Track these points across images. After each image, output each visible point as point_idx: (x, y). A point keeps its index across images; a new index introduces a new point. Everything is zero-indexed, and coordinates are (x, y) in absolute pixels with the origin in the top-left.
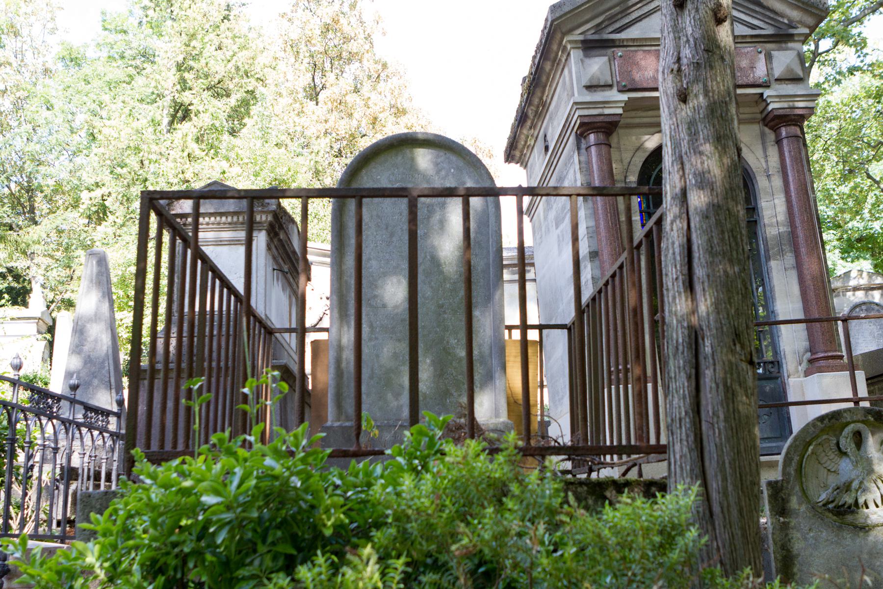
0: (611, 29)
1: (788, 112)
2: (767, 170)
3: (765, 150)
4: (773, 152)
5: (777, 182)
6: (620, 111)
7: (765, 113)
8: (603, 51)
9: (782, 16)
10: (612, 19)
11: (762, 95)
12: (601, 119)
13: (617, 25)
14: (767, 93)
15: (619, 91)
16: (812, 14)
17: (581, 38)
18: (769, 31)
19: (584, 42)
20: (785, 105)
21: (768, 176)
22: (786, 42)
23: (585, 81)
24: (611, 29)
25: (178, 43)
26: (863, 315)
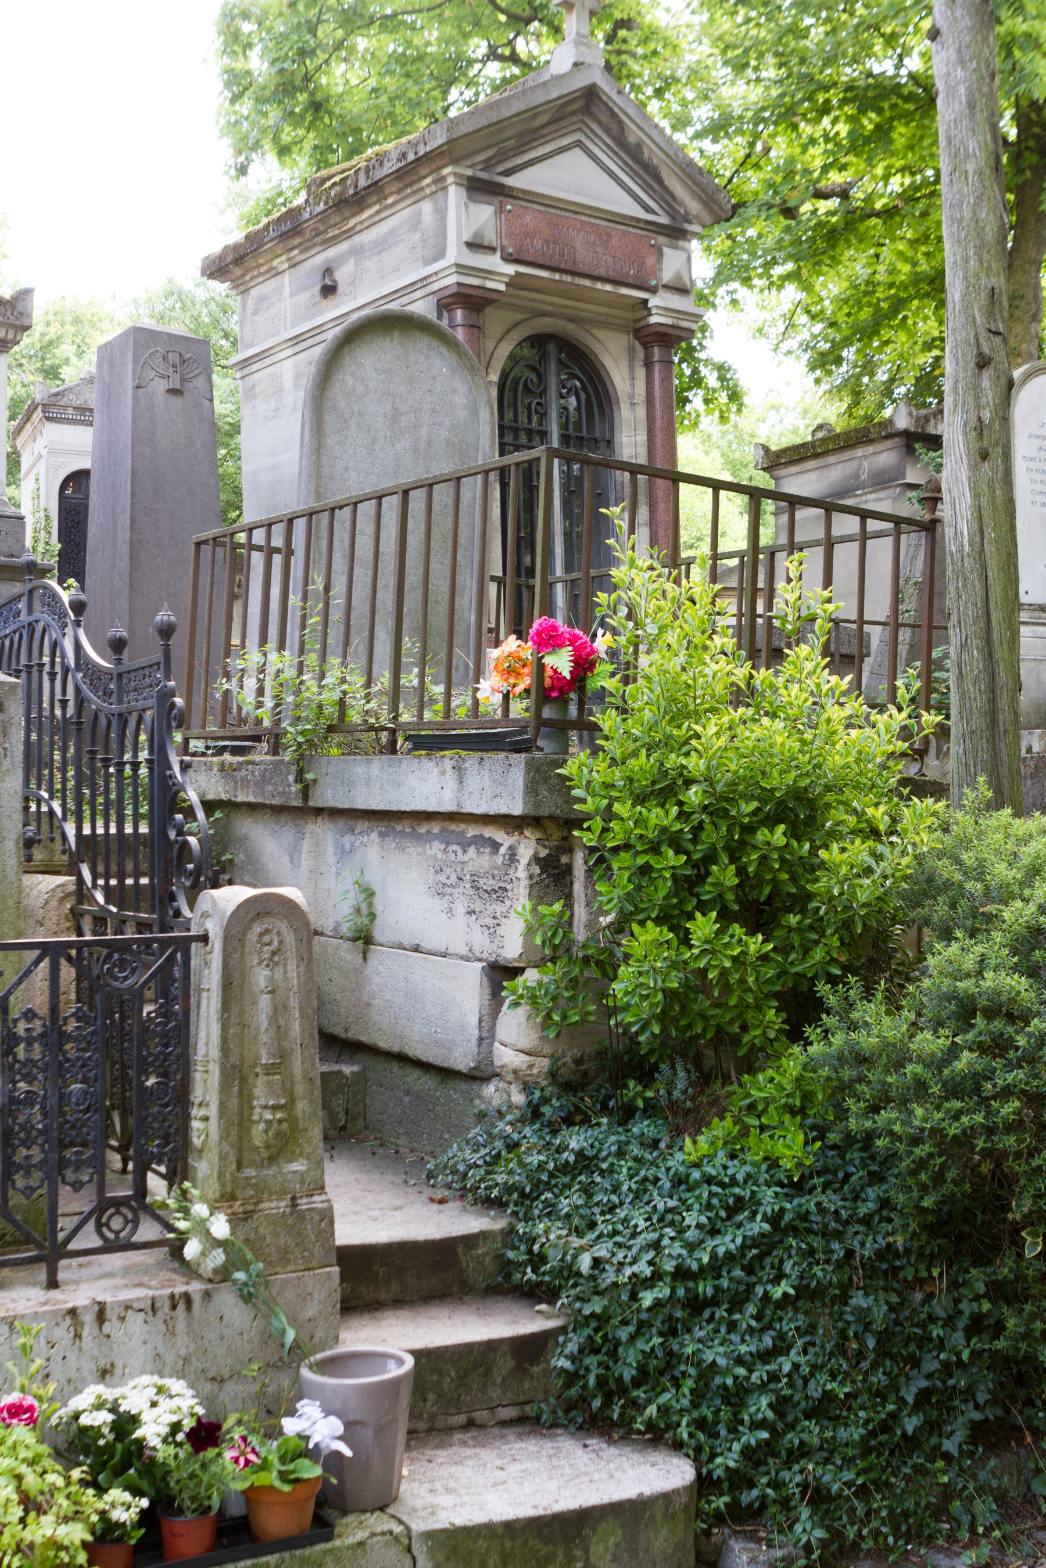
0: (500, 168)
1: (670, 331)
2: (631, 396)
3: (632, 369)
4: (641, 373)
5: (641, 413)
6: (502, 287)
7: (643, 323)
8: (489, 198)
9: (681, 204)
10: (504, 155)
11: (646, 301)
12: (480, 293)
13: (508, 165)
14: (654, 301)
15: (503, 259)
16: (711, 211)
17: (469, 172)
18: (664, 220)
19: (471, 179)
20: (669, 321)
21: (633, 404)
22: (677, 238)
23: (466, 237)
24: (500, 168)
25: (85, 1347)
26: (899, 683)
